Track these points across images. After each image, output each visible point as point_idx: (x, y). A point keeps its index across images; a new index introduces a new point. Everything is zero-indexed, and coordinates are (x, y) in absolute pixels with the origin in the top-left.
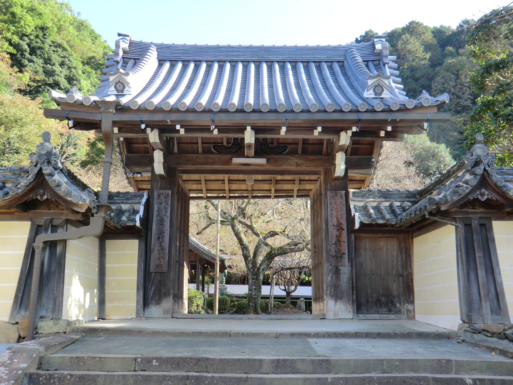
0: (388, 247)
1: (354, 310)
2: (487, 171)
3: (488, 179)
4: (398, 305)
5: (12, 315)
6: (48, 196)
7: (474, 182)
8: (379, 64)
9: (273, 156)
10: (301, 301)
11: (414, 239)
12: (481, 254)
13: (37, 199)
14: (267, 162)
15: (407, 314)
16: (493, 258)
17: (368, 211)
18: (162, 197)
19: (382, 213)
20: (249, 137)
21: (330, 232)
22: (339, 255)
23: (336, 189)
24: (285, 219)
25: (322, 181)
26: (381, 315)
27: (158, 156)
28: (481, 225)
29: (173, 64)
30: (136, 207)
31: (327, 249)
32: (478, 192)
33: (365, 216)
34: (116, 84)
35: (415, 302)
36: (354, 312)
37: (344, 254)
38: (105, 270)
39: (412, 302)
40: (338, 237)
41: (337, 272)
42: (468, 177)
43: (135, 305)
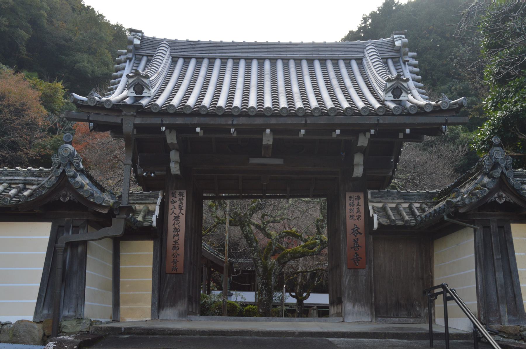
2: (505, 174)
4: (418, 309)
6: (70, 197)
7: (492, 186)
8: (399, 62)
10: (314, 309)
12: (499, 257)
20: (268, 138)
27: (174, 156)
28: (498, 227)
29: (187, 60)
30: (151, 207)
32: (496, 195)
33: (384, 218)
34: (135, 86)
36: (372, 314)
38: (119, 271)
42: (486, 180)
43: (150, 306)
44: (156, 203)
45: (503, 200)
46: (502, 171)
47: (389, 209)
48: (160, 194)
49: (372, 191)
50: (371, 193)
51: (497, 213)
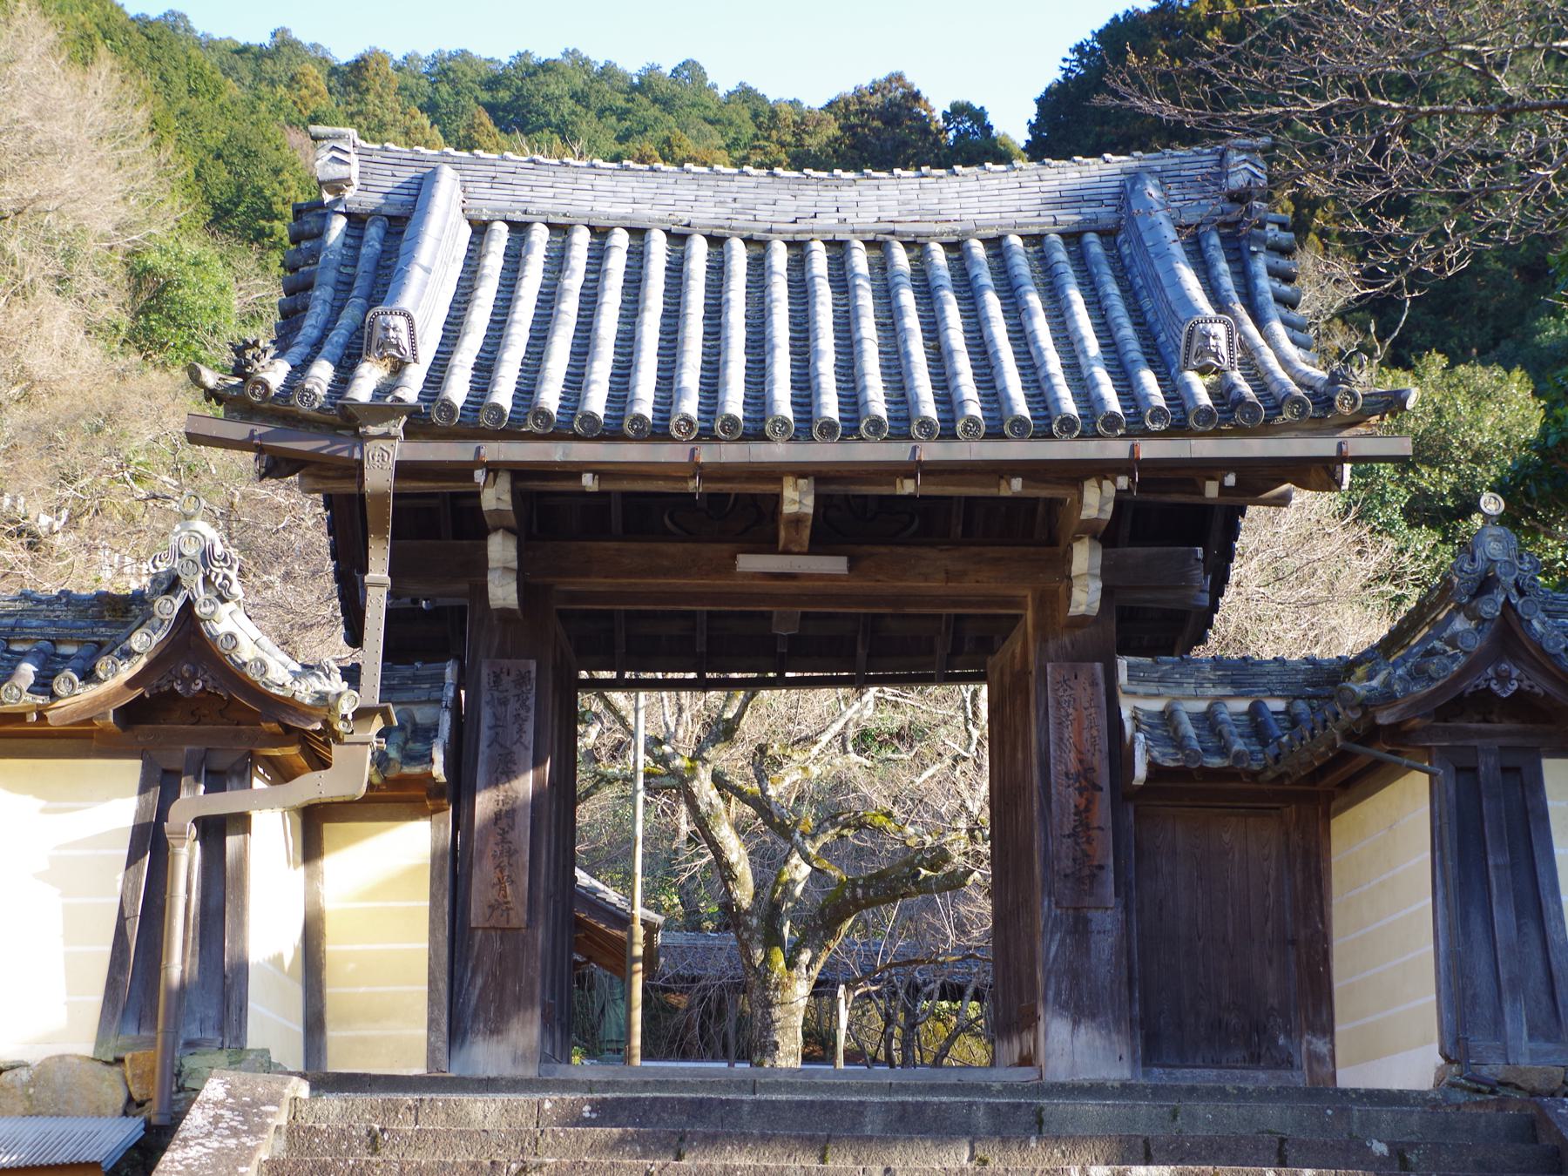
0: (1250, 846)
1: (1134, 1053)
3: (1517, 629)
4: (1281, 1041)
5: (100, 1041)
7: (1476, 643)
9: (867, 548)
11: (1333, 822)
12: (1504, 859)
13: (173, 690)
14: (850, 569)
15: (1310, 1070)
16: (1541, 869)
17: (1176, 730)
18: (506, 681)
19: (1220, 735)
20: (797, 499)
21: (1054, 798)
22: (1086, 872)
23: (1078, 656)
24: (911, 759)
25: (1030, 629)
26: (1222, 1072)
27: (501, 550)
28: (1504, 770)
31: (1046, 851)
32: (1490, 671)
33: (1166, 745)
35: (1338, 1029)
36: (1134, 1061)
37: (1101, 867)
39: (1328, 1030)
40: (1084, 813)
41: (1080, 928)
42: (1460, 624)
43: (423, 1032)
44: (439, 701)
45: (1514, 686)
46: (1507, 599)
47: (1185, 718)
48: (448, 670)
49: (1132, 659)
50: (1129, 667)
51: (1499, 727)
